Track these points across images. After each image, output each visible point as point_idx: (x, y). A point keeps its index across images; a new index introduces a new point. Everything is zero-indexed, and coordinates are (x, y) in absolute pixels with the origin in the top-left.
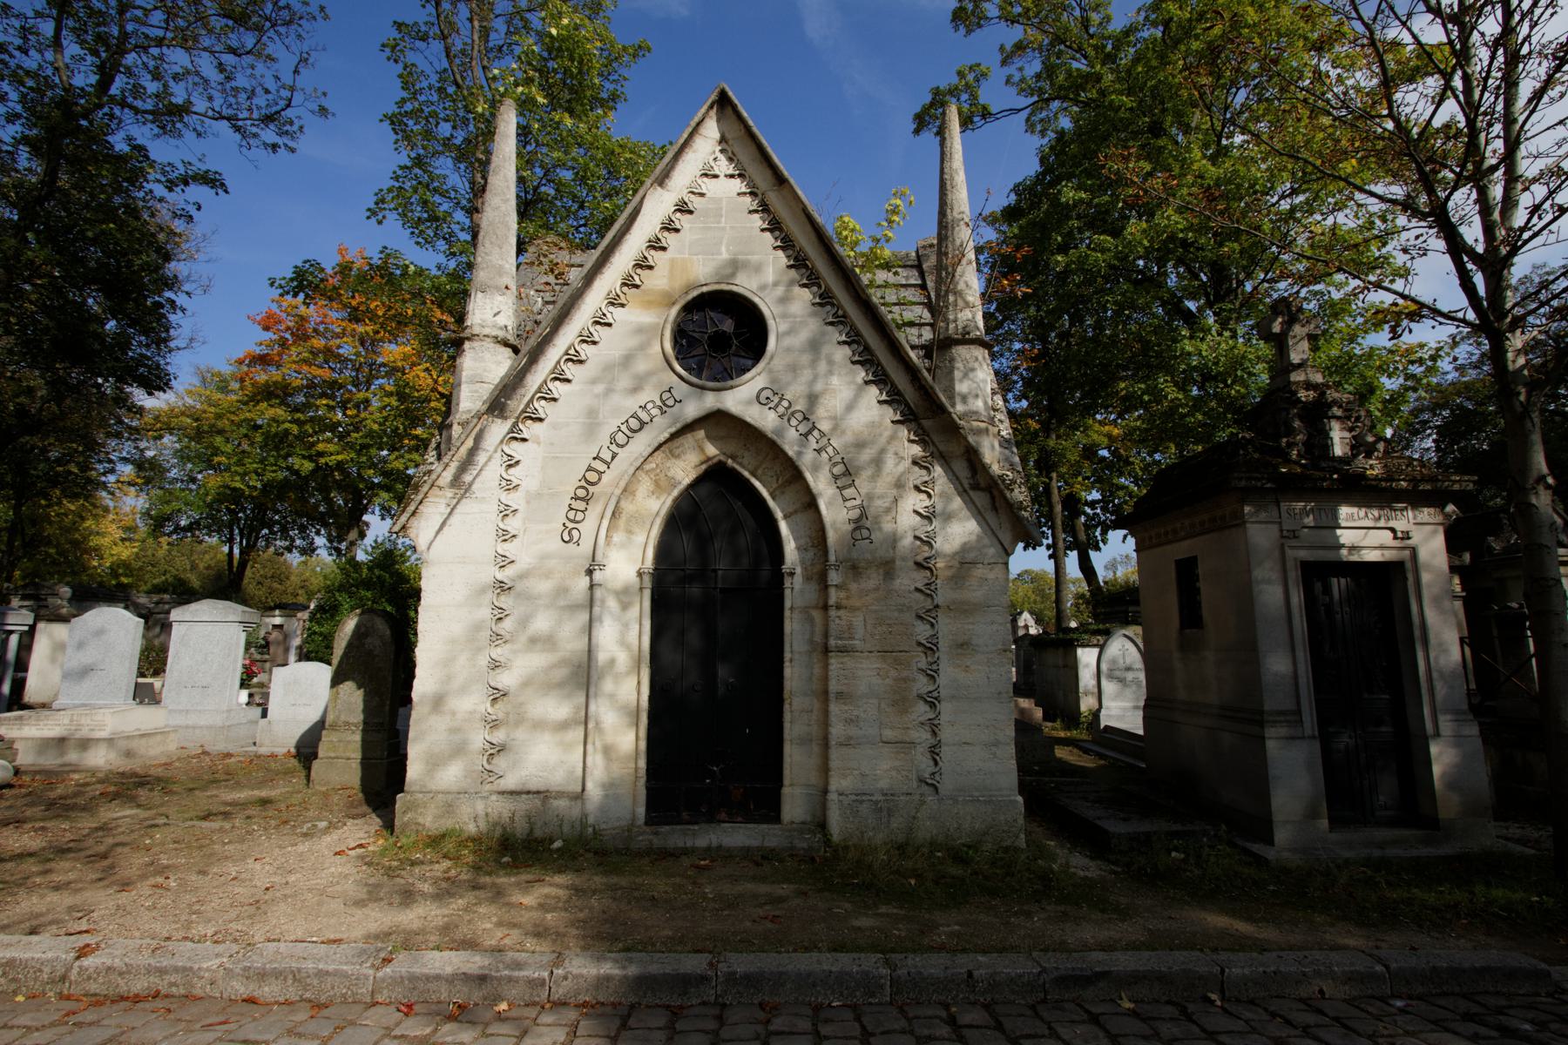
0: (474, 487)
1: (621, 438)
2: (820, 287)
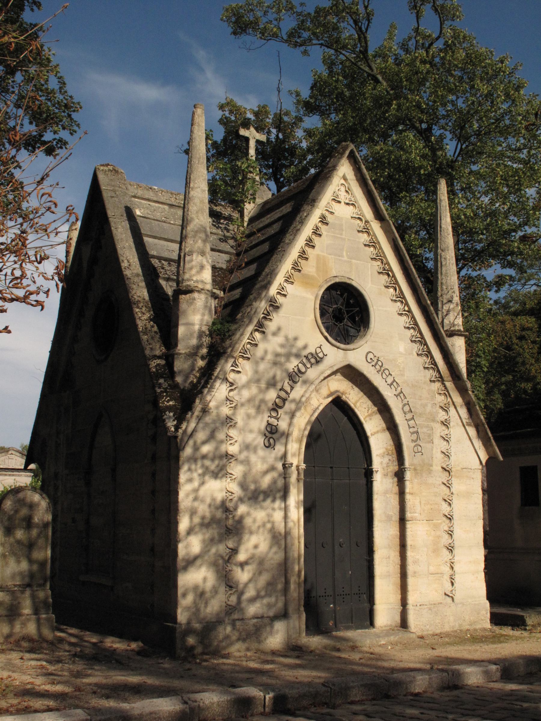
2: (395, 290)
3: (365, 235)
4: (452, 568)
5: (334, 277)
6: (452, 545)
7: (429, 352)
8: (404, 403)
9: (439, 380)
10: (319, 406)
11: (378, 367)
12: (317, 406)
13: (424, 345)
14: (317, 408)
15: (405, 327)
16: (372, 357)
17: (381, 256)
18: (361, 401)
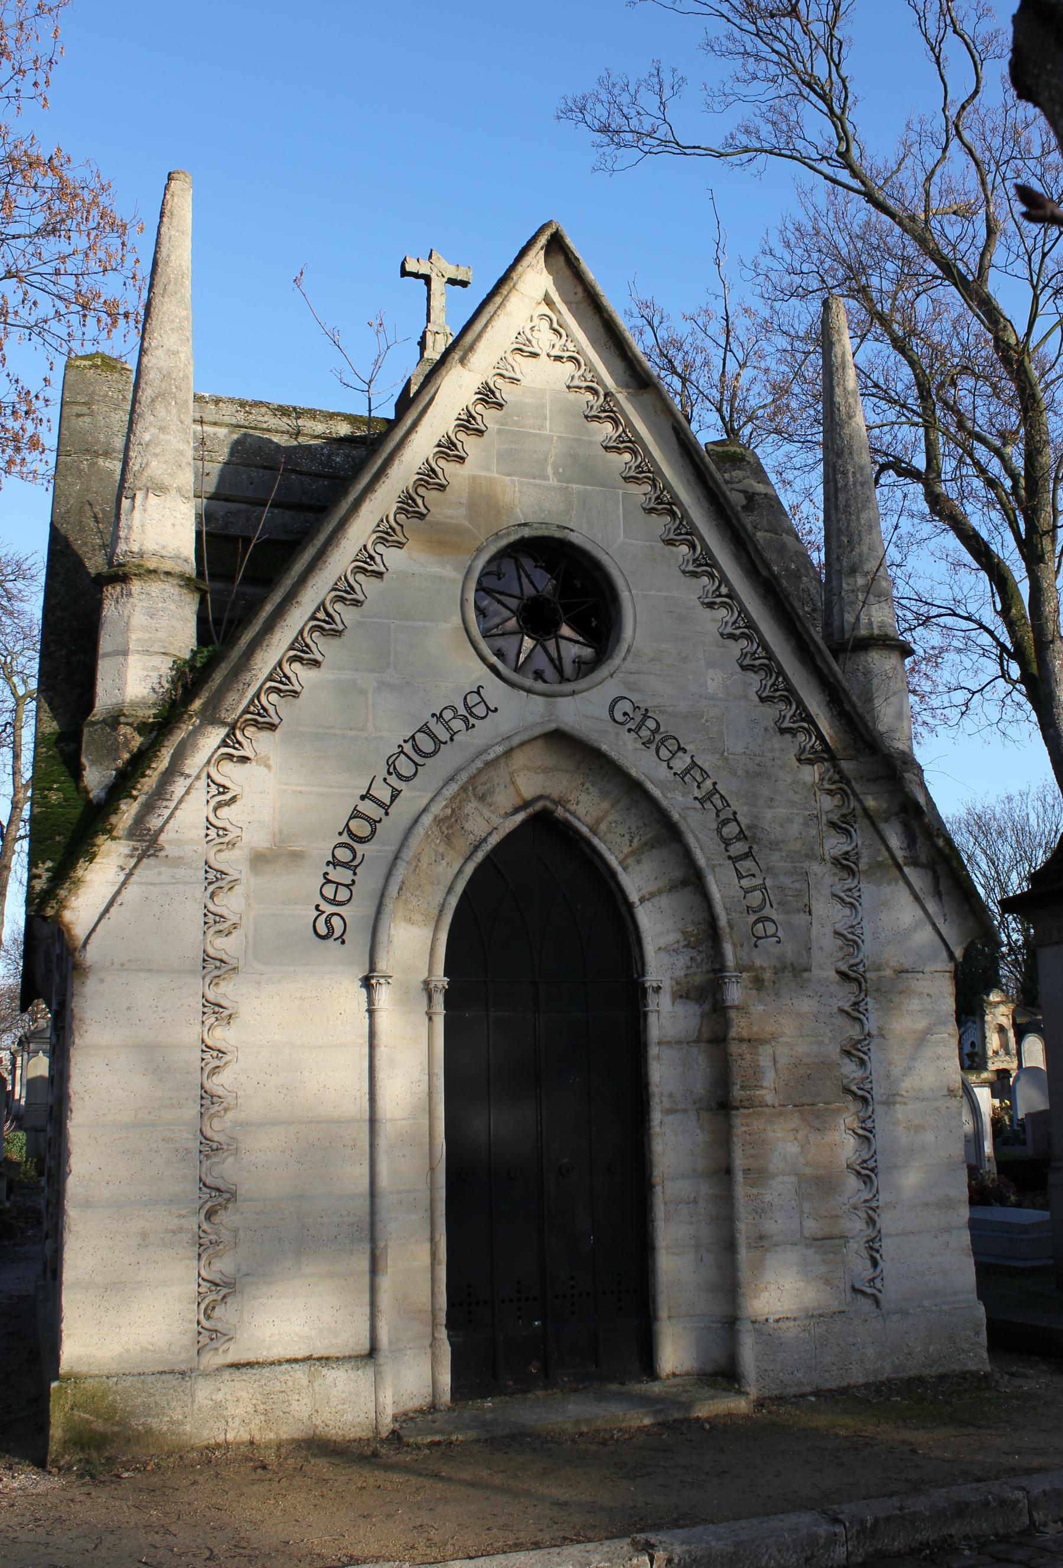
0: (162, 838)
1: (405, 767)
2: (693, 547)
3: (609, 427)
4: (871, 1222)
5: (519, 525)
6: (871, 1164)
7: (790, 689)
8: (722, 817)
9: (824, 759)
10: (490, 834)
11: (645, 733)
12: (484, 835)
13: (778, 674)
14: (484, 840)
15: (722, 635)
16: (627, 706)
17: (649, 471)
18: (610, 818)
